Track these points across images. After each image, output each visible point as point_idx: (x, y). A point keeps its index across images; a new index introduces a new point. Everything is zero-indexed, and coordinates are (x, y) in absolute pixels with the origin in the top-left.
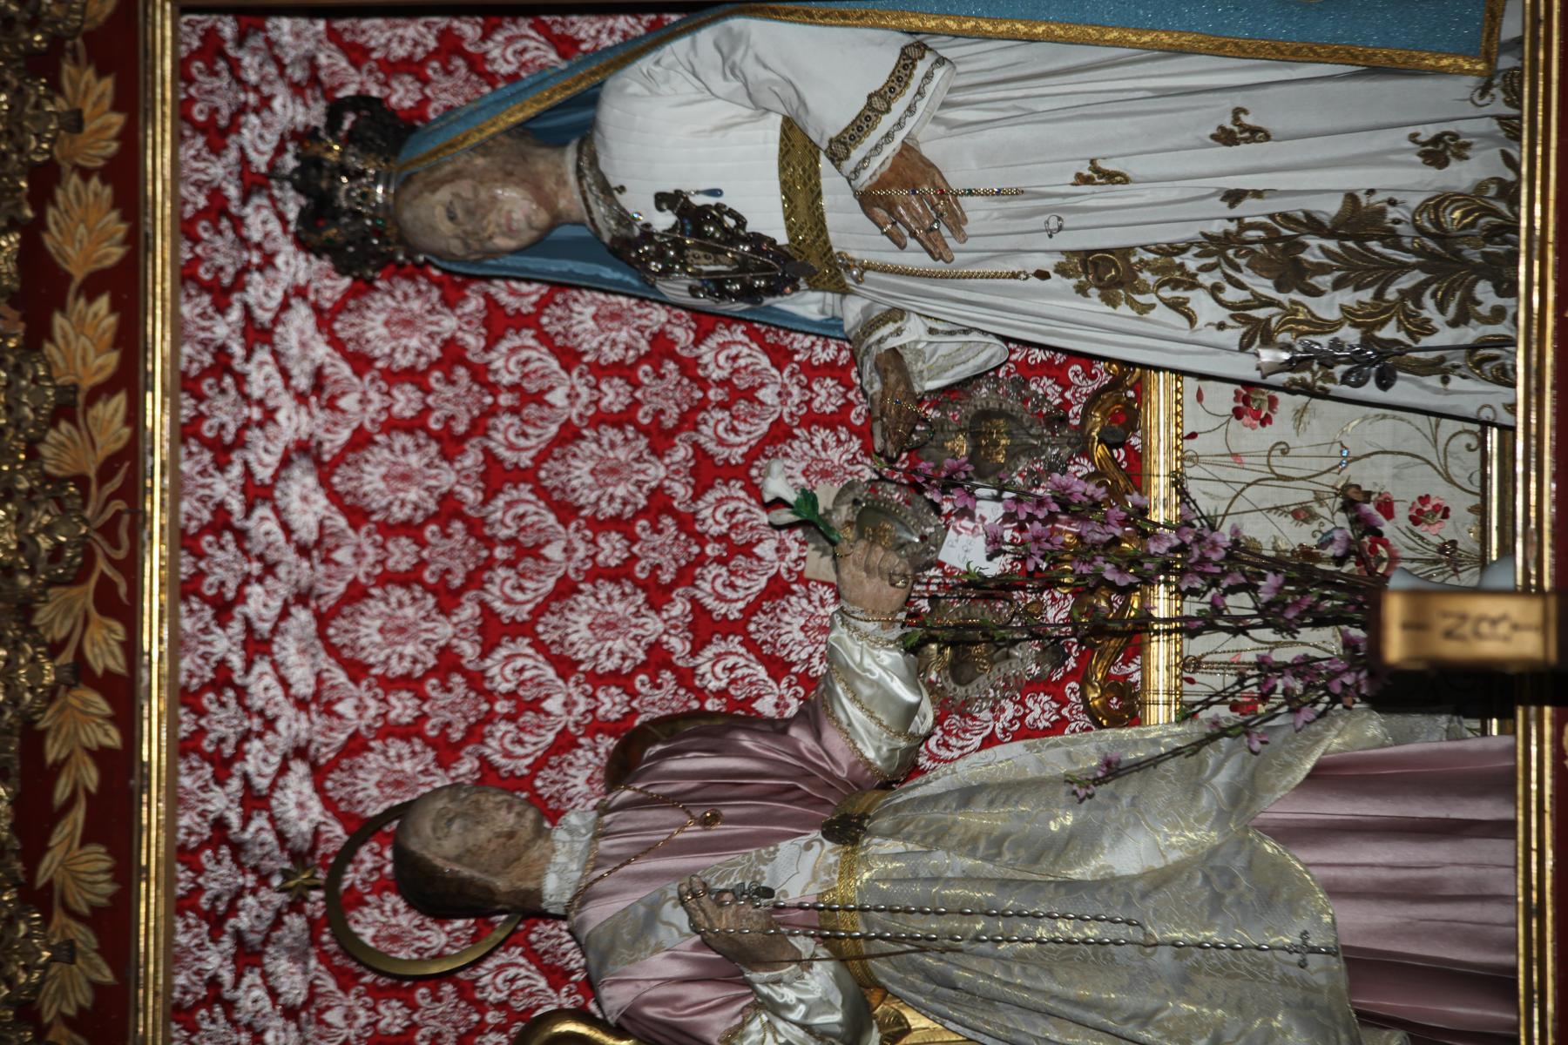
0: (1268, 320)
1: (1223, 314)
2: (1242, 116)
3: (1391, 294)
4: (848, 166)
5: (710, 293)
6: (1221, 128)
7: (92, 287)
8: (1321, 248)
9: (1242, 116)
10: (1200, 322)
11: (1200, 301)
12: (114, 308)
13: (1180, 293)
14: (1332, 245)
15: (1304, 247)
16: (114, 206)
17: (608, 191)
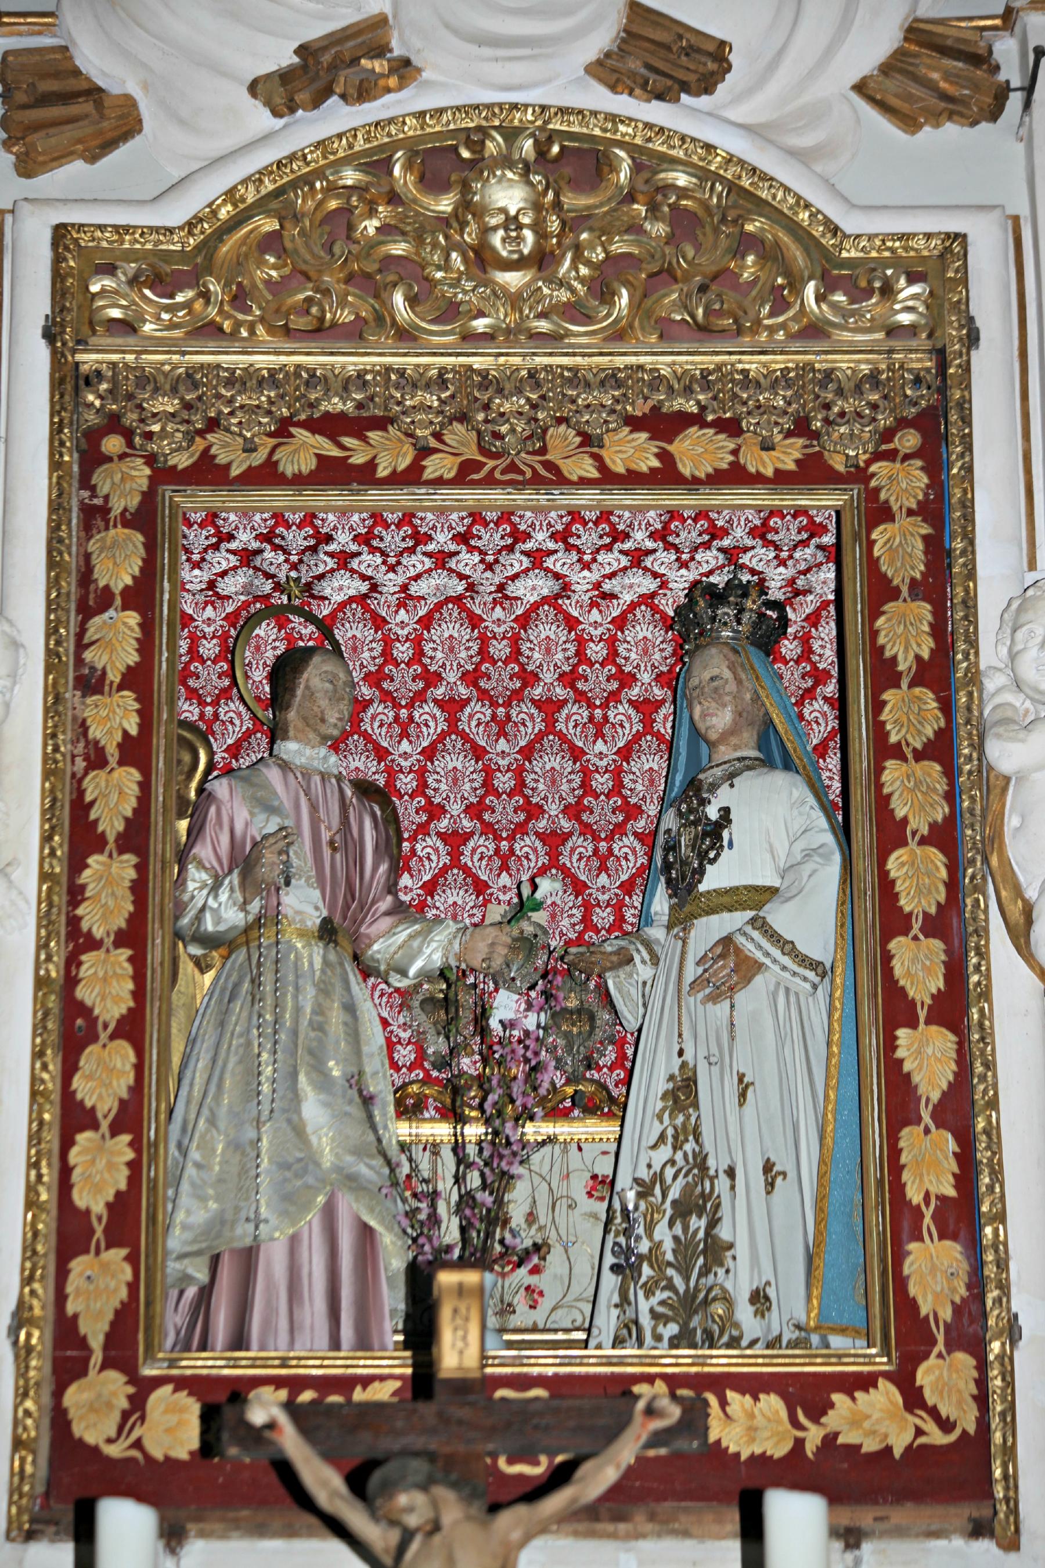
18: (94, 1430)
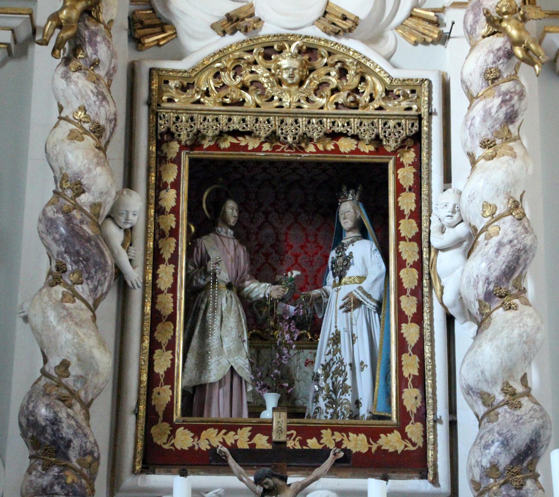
18: (160, 440)
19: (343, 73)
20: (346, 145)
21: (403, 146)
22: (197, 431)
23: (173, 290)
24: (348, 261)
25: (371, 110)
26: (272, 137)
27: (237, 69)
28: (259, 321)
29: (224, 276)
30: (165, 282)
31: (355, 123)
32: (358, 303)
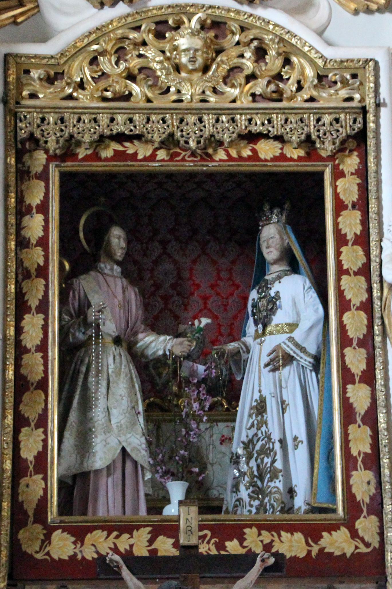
0: (249, 448)
1: (250, 437)
2: (300, 443)
3: (255, 479)
4: (287, 342)
5: (253, 304)
6: (298, 438)
7: (254, 150)
8: (267, 462)
9: (300, 443)
10: (248, 431)
11: (254, 430)
12: (249, 156)
13: (256, 426)
14: (269, 465)
15: (268, 458)
16: (274, 156)
17: (279, 278)
18: (31, 548)
19: (261, 53)
20: (267, 150)
21: (342, 149)
22: (79, 534)
23: (43, 347)
24: (273, 305)
25: (299, 102)
26: (169, 142)
27: (120, 53)
28: (157, 384)
29: (110, 327)
30: (32, 337)
31: (278, 119)
32: (288, 359)
